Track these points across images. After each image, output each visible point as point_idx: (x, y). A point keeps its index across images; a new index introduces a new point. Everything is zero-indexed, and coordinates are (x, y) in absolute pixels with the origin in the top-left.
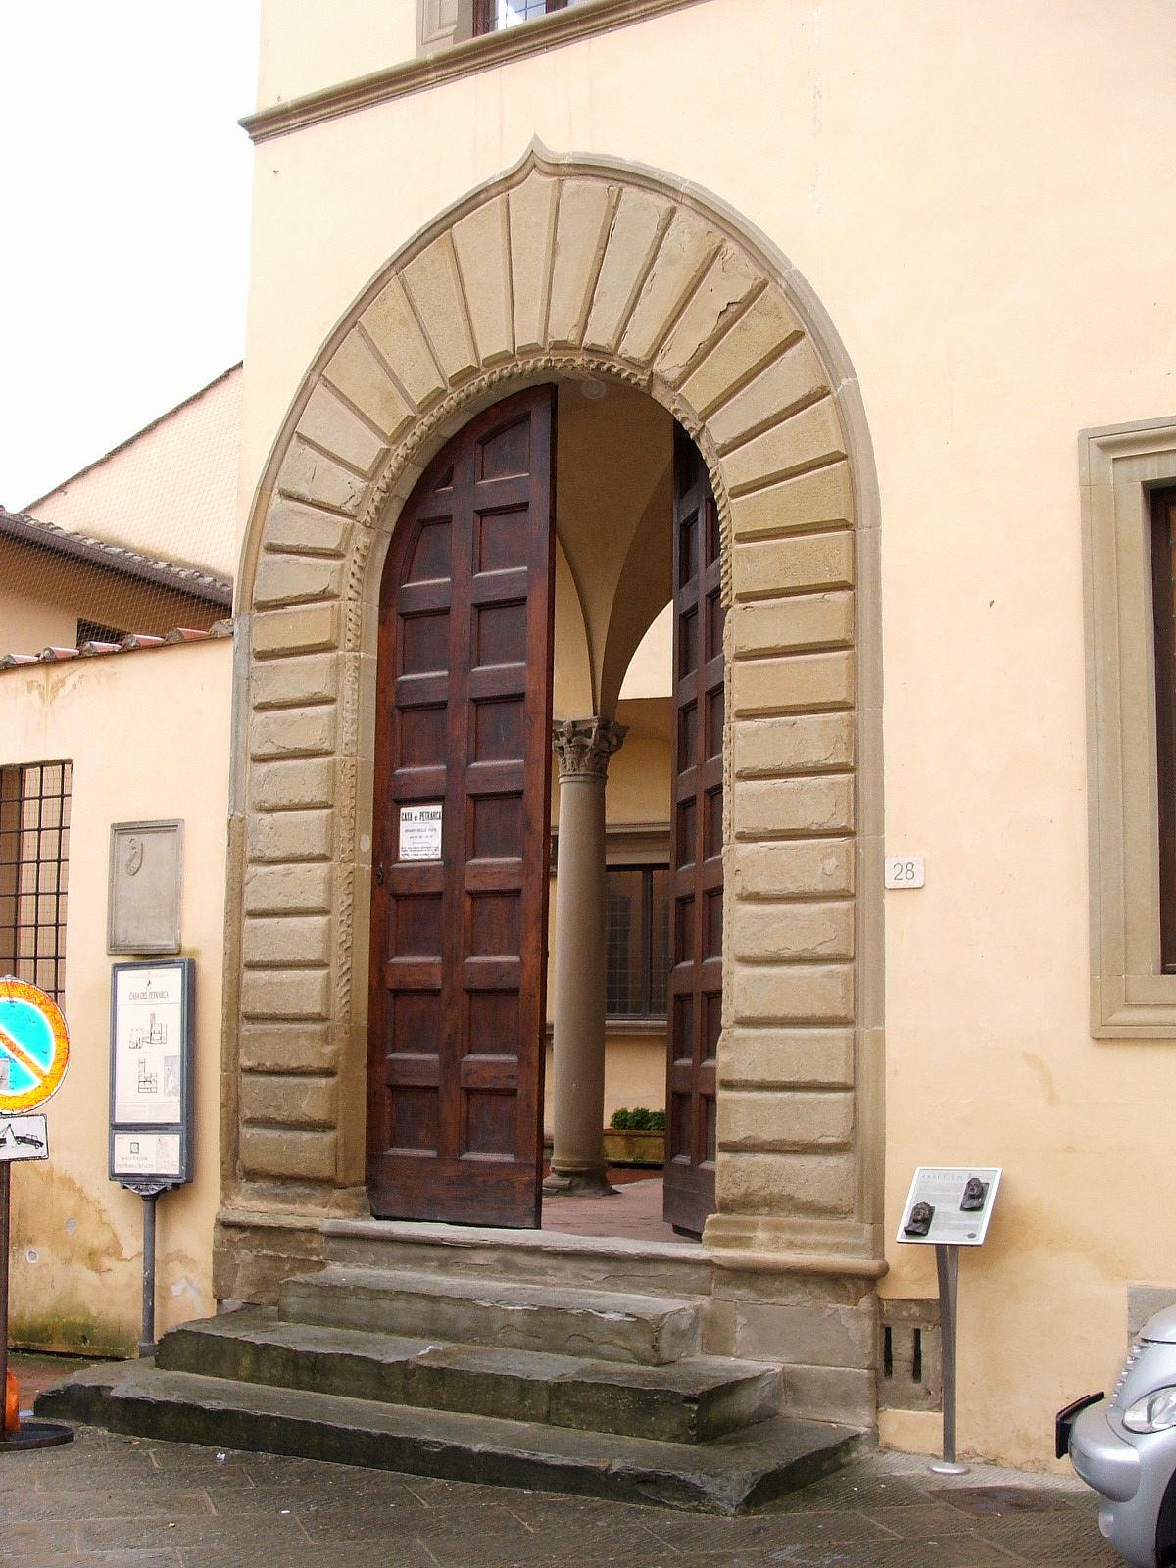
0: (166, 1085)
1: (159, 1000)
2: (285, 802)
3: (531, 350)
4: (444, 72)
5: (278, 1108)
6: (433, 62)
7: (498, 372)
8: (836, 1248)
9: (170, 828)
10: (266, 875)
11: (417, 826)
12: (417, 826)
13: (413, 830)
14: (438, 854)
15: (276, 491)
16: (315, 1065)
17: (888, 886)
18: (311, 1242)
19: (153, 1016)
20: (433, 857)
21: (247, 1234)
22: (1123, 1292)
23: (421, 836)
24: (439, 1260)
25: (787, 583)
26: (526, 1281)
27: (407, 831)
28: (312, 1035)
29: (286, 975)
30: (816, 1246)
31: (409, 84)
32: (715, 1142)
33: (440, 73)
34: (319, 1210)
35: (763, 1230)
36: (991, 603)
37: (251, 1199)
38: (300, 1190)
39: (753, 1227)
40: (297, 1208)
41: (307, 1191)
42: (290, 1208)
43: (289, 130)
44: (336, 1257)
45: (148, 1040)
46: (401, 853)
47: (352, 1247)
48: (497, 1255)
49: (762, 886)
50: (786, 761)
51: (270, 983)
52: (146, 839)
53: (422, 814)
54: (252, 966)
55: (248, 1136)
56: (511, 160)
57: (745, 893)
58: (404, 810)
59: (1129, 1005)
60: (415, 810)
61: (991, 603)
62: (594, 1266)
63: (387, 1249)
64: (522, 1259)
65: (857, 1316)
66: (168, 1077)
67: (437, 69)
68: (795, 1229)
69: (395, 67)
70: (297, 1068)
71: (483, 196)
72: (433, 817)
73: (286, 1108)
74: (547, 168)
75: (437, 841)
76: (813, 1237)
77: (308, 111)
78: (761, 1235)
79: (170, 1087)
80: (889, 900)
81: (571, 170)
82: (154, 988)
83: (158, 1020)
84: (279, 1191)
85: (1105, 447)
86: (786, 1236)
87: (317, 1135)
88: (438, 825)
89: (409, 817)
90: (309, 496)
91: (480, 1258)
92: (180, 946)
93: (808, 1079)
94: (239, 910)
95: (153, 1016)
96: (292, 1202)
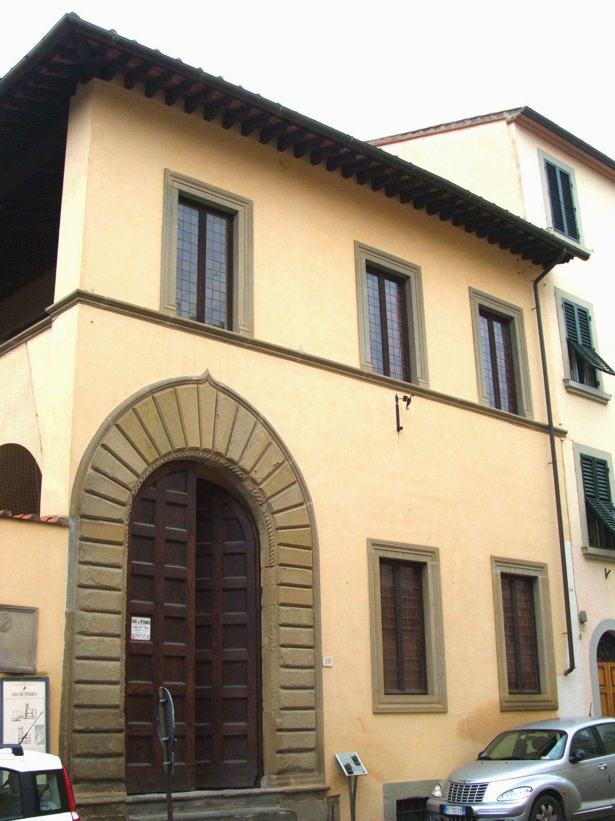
0: (36, 739)
1: (33, 697)
2: (100, 608)
3: (206, 451)
4: (174, 324)
5: (96, 748)
6: (172, 319)
7: (192, 453)
8: (314, 782)
9: (32, 611)
10: (90, 640)
11: (139, 626)
12: (139, 626)
13: (137, 627)
14: (149, 638)
15: (90, 466)
16: (117, 727)
17: (324, 665)
18: (118, 808)
19: (27, 705)
20: (147, 639)
21: (83, 809)
22: (381, 785)
23: (142, 630)
24: (179, 807)
25: (296, 563)
26: (218, 810)
27: (134, 627)
28: (115, 714)
29: (100, 687)
30: (309, 782)
31: (159, 320)
32: (126, 756)
33: (172, 324)
34: (118, 793)
35: (292, 779)
36: (347, 583)
37: (80, 792)
38: (105, 785)
39: (289, 778)
40: (106, 793)
41: (109, 785)
42: (104, 794)
43: (99, 307)
44: (130, 813)
45: (25, 717)
46: (132, 636)
47: (140, 807)
48: (203, 801)
49: (290, 663)
50: (296, 622)
51: (92, 690)
52: (13, 615)
53: (141, 621)
54: (79, 682)
55: (78, 762)
56: (198, 373)
57: (284, 665)
58: (133, 618)
59: (381, 703)
60: (138, 619)
61: (347, 583)
62: (240, 799)
63: (154, 806)
64: (214, 801)
65: (323, 803)
66: (38, 736)
67: (172, 322)
68: (301, 778)
69: (144, 308)
70: (107, 729)
71: (187, 382)
72: (146, 622)
73: (101, 748)
74: (212, 383)
75: (148, 633)
76: (307, 780)
77: (111, 305)
78: (292, 781)
79: (39, 740)
80: (323, 669)
81: (221, 389)
82: (27, 690)
83: (30, 707)
84: (94, 787)
85: (373, 544)
86: (299, 780)
87: (115, 759)
88: (149, 626)
89: (135, 621)
90: (110, 474)
91: (198, 803)
92: (35, 669)
93: (305, 727)
94: (71, 655)
95: (27, 705)
96: (103, 791)
